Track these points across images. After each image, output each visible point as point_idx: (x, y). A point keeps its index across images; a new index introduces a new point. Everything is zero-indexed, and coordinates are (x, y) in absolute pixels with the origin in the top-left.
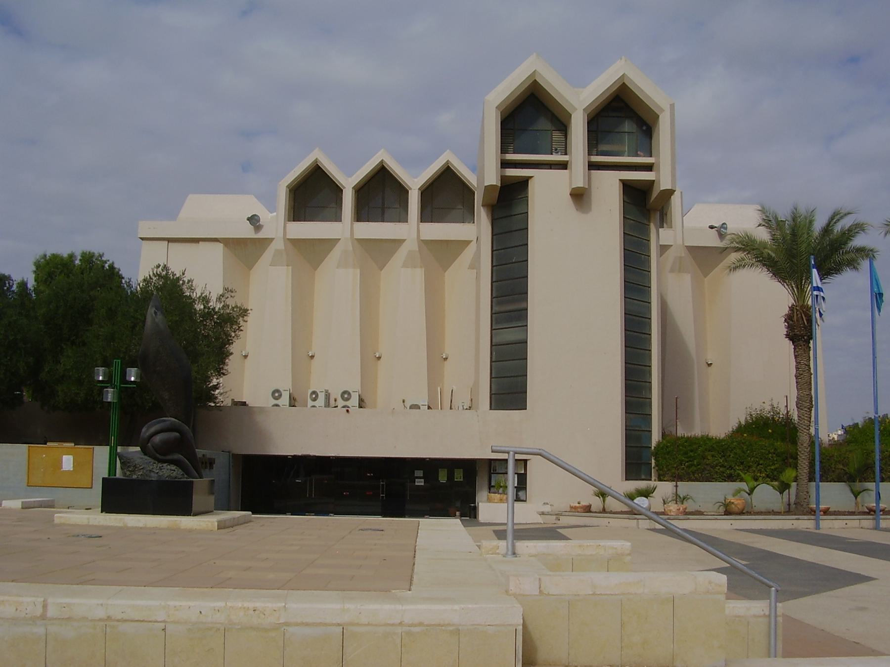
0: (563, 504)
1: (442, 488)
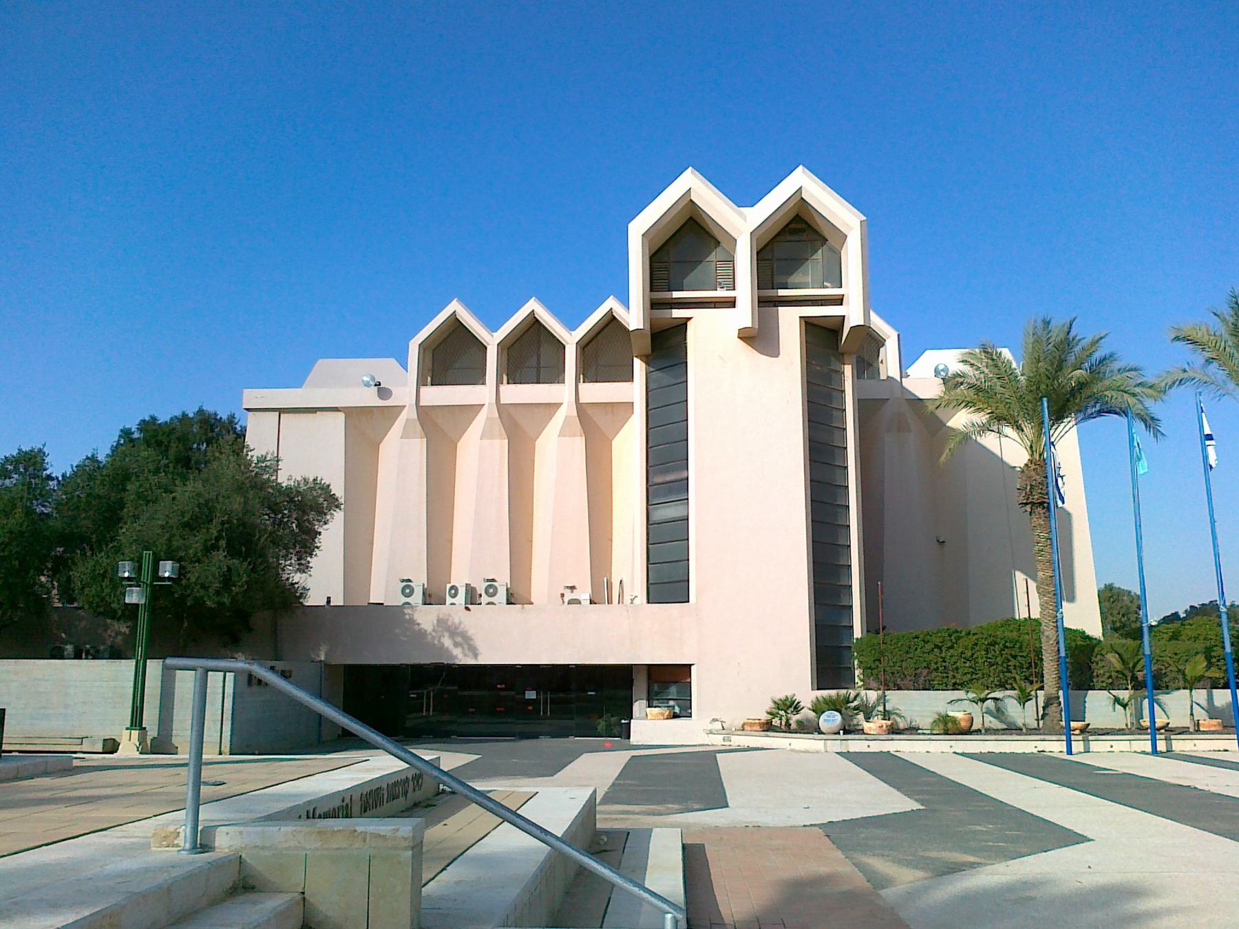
0: (735, 718)
1: (589, 699)
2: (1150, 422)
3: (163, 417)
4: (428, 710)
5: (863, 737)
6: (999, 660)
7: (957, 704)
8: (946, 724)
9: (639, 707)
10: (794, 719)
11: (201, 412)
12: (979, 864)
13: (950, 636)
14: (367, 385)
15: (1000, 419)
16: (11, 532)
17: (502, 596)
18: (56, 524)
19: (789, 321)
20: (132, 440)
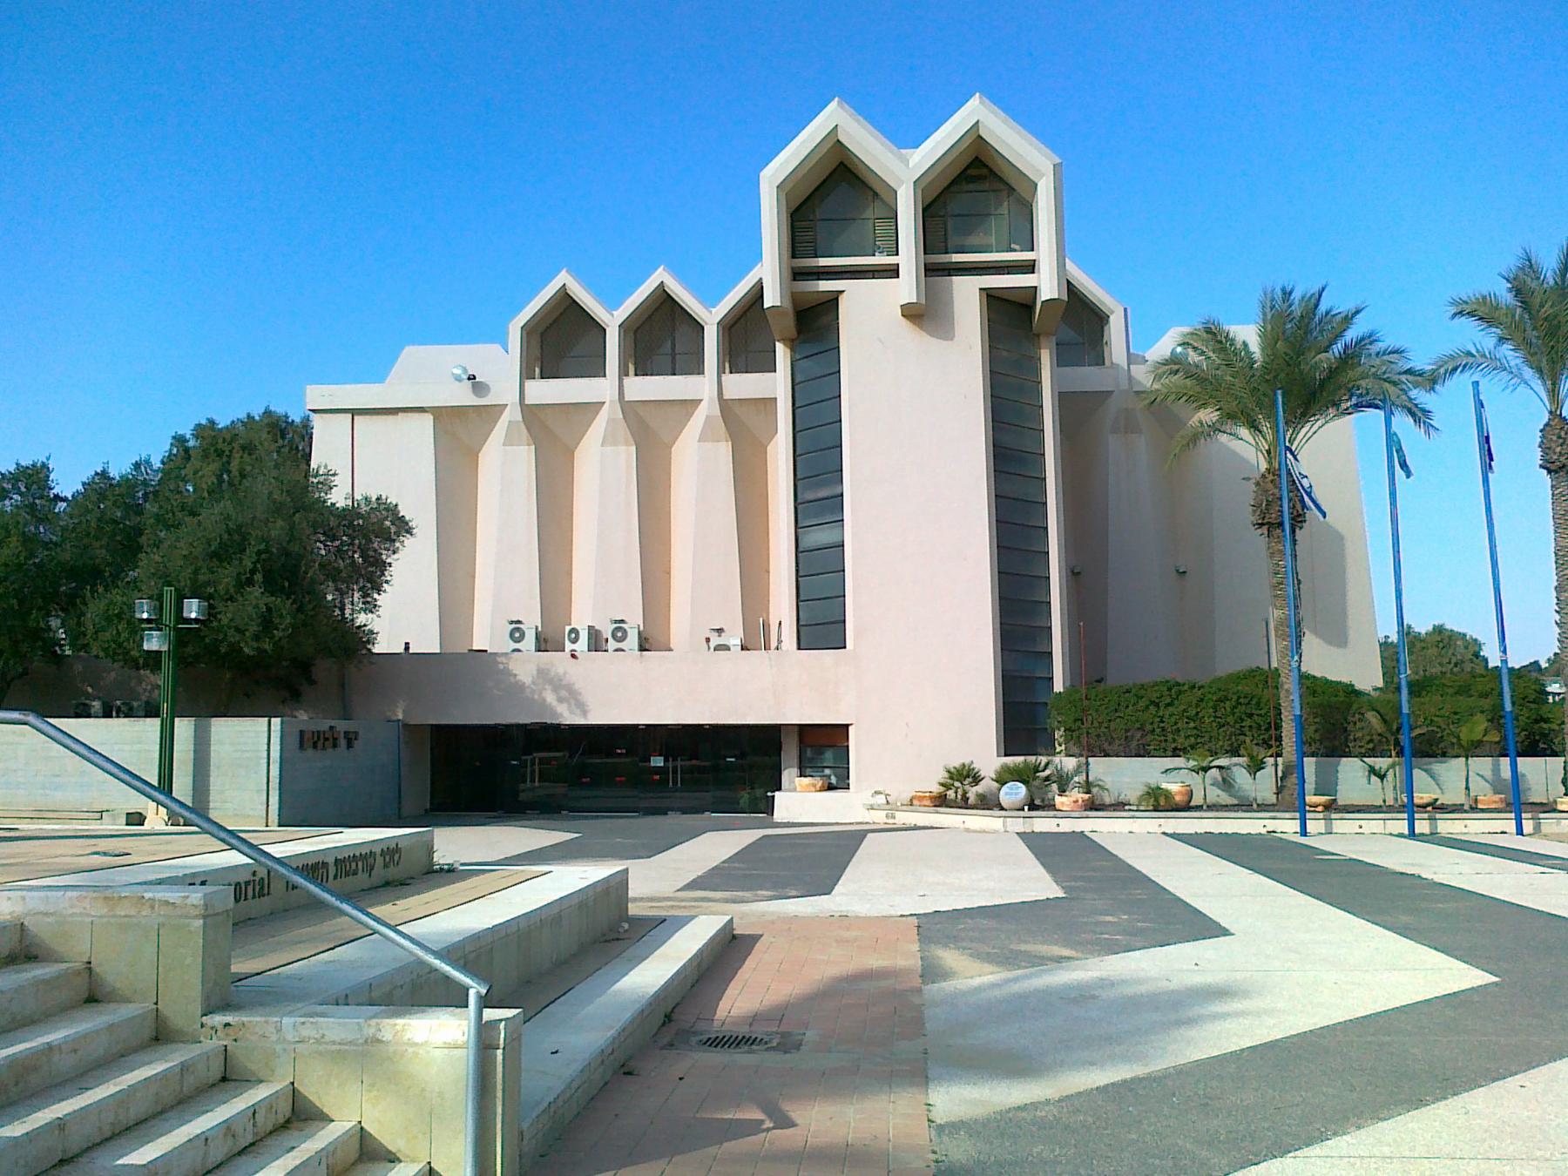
1: (725, 767)
2: (1420, 415)
3: (223, 422)
4: (533, 781)
5: (1052, 813)
6: (1230, 719)
7: (1169, 774)
8: (1156, 800)
9: (789, 775)
10: (973, 792)
11: (268, 413)
12: (1069, 958)
13: (1169, 689)
14: (458, 379)
15: (1231, 416)
16: (6, 565)
17: (632, 641)
18: (66, 555)
19: (966, 294)
20: (187, 450)
